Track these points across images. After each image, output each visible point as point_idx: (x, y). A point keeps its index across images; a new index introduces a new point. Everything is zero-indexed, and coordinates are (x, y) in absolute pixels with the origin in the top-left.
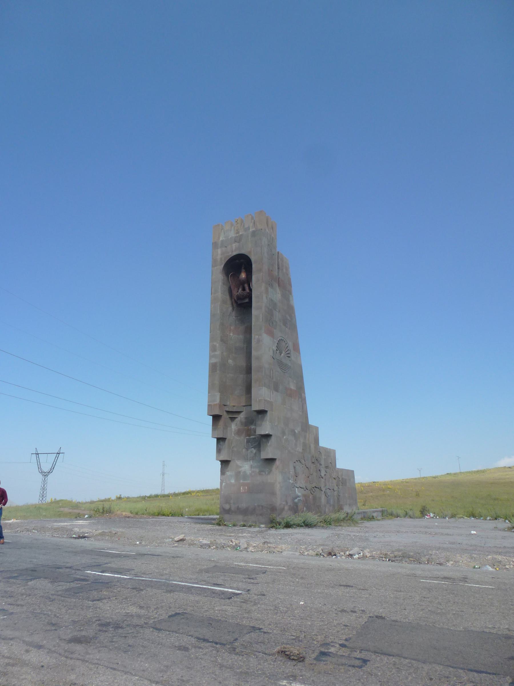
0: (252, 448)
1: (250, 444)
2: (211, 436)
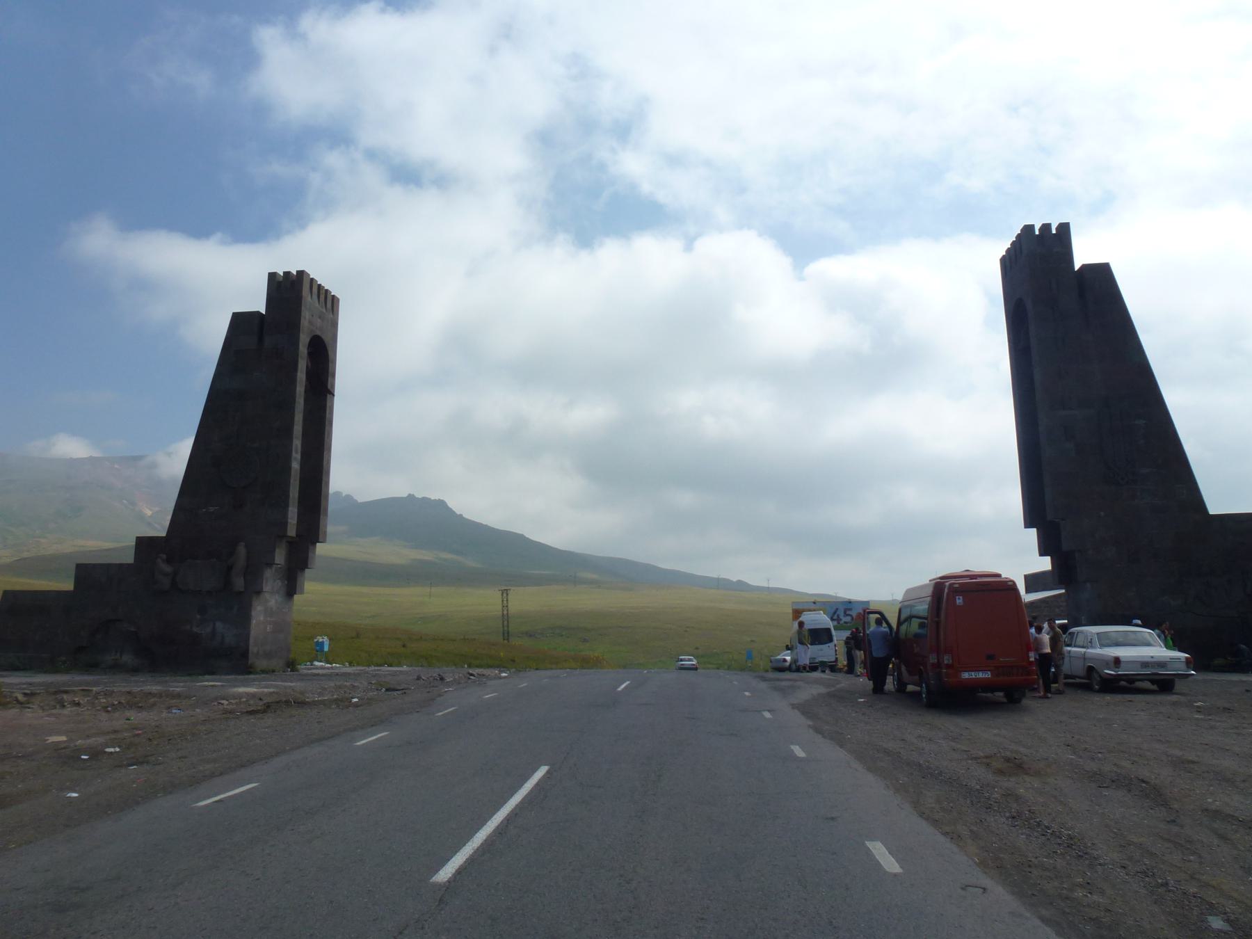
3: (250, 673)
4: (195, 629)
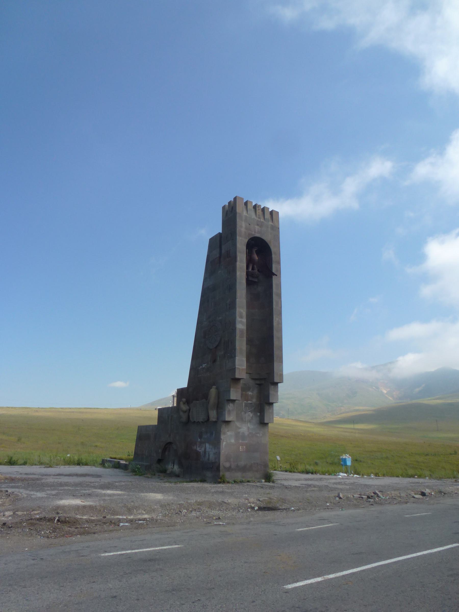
0: (249, 412)
1: (248, 408)
2: (178, 388)
3: (220, 483)
4: (198, 449)
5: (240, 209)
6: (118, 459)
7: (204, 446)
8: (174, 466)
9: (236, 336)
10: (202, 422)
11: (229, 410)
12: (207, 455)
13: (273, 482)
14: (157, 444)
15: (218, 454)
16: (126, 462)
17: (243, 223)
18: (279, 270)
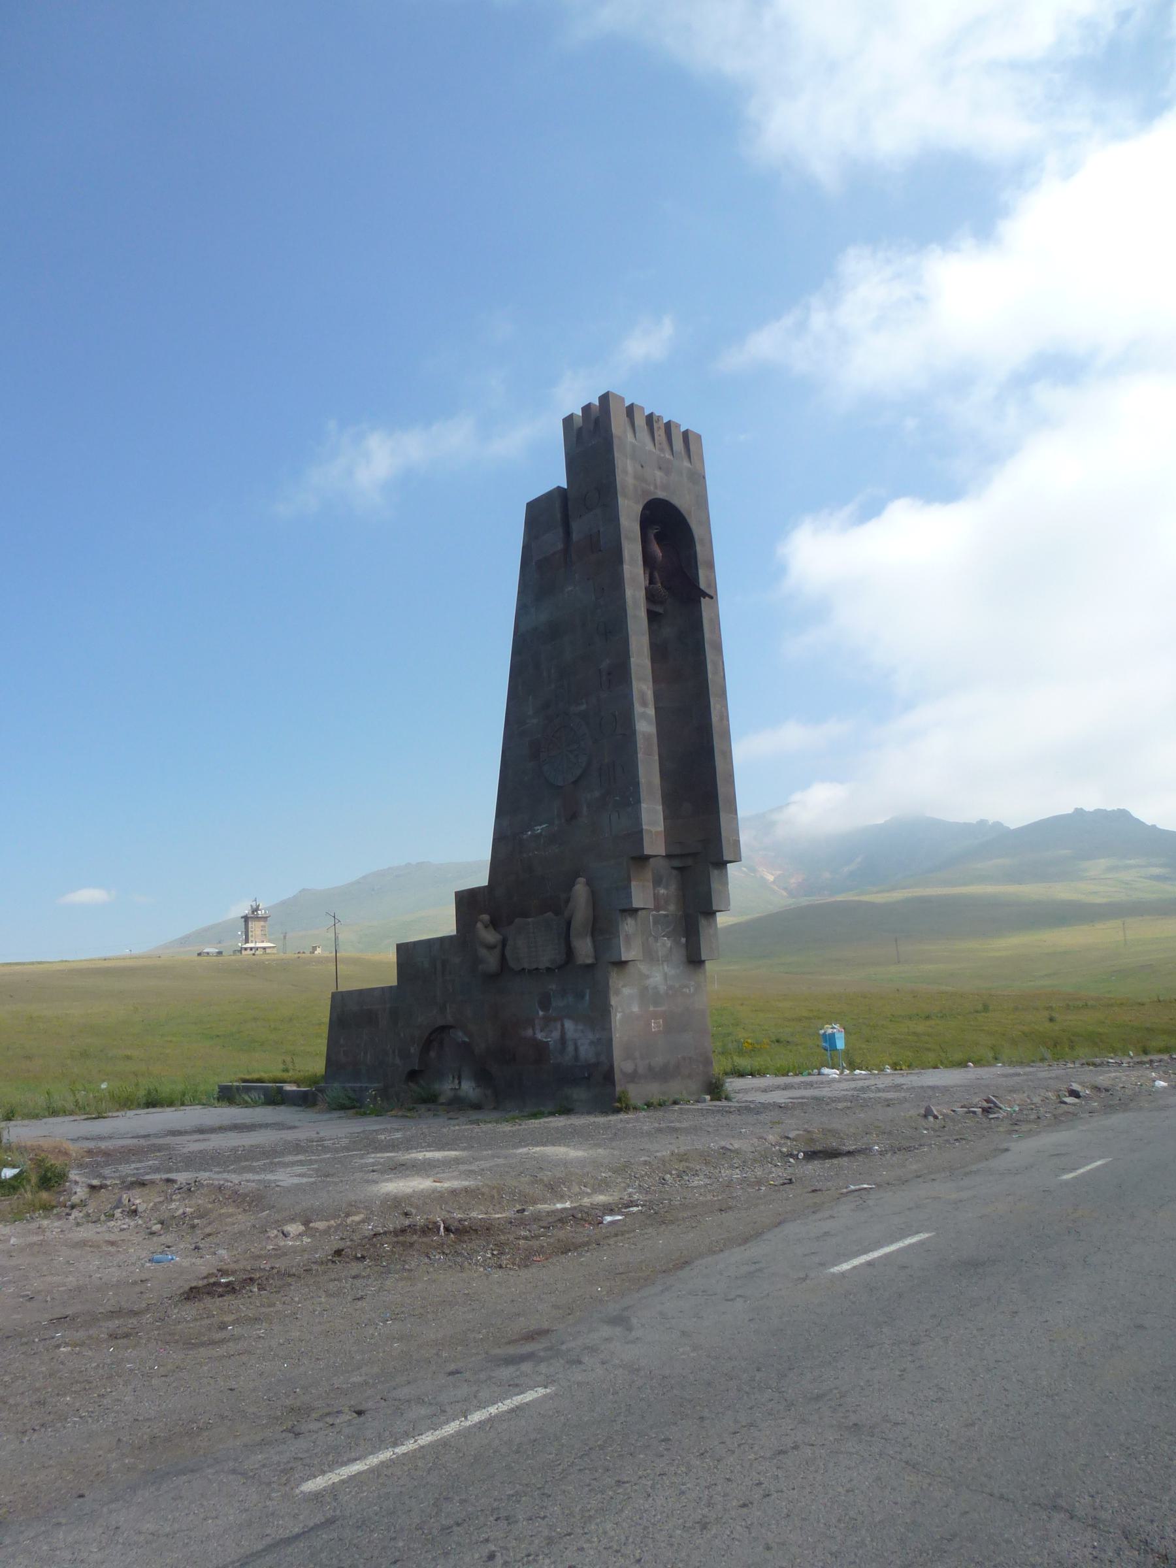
0: (664, 936)
1: (660, 927)
3: (618, 1111)
4: (540, 1036)
5: (618, 423)
6: (270, 1082)
7: (559, 1026)
8: (460, 1083)
9: (637, 753)
10: (548, 969)
11: (627, 935)
12: (570, 1048)
13: (727, 1099)
14: (402, 1035)
15: (606, 1044)
16: (299, 1087)
17: (628, 461)
18: (713, 584)
